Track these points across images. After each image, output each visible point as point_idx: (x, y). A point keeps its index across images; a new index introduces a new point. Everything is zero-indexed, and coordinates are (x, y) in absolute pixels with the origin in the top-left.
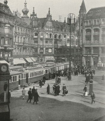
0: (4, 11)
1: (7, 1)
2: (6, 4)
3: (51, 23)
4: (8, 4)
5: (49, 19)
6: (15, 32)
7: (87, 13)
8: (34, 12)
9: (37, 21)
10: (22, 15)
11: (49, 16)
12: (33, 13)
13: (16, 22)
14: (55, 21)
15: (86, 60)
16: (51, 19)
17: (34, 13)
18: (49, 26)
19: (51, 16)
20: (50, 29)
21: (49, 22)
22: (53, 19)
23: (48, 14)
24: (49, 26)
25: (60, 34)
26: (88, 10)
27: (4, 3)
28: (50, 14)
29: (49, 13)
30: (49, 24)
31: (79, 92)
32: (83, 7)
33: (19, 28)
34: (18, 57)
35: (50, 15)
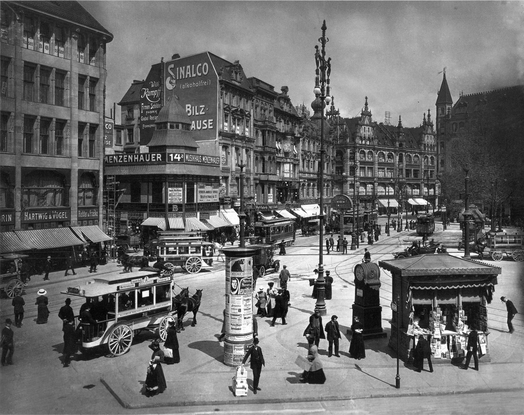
0: (282, 108)
1: (287, 87)
2: (286, 93)
3: (370, 128)
4: (288, 94)
5: (366, 122)
6: (302, 150)
7: (453, 105)
8: (334, 107)
9: (341, 125)
10: (312, 113)
11: (366, 114)
12: (331, 108)
13: (303, 130)
14: (378, 123)
15: (131, 115)
16: (370, 120)
17: (334, 109)
18: (367, 136)
19: (370, 115)
20: (368, 143)
21: (367, 128)
22: (374, 119)
23: (364, 110)
24: (367, 136)
25: (391, 152)
26: (455, 99)
27: (281, 92)
28: (369, 110)
29: (366, 108)
30: (366, 131)
31: (148, 190)
32: (444, 94)
33: (310, 143)
34: (456, 275)
35: (430, 122)
